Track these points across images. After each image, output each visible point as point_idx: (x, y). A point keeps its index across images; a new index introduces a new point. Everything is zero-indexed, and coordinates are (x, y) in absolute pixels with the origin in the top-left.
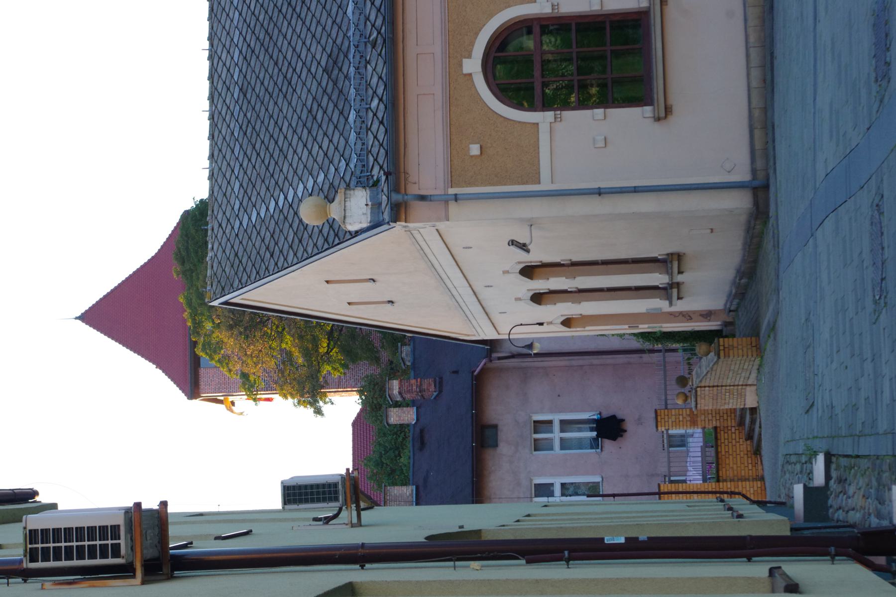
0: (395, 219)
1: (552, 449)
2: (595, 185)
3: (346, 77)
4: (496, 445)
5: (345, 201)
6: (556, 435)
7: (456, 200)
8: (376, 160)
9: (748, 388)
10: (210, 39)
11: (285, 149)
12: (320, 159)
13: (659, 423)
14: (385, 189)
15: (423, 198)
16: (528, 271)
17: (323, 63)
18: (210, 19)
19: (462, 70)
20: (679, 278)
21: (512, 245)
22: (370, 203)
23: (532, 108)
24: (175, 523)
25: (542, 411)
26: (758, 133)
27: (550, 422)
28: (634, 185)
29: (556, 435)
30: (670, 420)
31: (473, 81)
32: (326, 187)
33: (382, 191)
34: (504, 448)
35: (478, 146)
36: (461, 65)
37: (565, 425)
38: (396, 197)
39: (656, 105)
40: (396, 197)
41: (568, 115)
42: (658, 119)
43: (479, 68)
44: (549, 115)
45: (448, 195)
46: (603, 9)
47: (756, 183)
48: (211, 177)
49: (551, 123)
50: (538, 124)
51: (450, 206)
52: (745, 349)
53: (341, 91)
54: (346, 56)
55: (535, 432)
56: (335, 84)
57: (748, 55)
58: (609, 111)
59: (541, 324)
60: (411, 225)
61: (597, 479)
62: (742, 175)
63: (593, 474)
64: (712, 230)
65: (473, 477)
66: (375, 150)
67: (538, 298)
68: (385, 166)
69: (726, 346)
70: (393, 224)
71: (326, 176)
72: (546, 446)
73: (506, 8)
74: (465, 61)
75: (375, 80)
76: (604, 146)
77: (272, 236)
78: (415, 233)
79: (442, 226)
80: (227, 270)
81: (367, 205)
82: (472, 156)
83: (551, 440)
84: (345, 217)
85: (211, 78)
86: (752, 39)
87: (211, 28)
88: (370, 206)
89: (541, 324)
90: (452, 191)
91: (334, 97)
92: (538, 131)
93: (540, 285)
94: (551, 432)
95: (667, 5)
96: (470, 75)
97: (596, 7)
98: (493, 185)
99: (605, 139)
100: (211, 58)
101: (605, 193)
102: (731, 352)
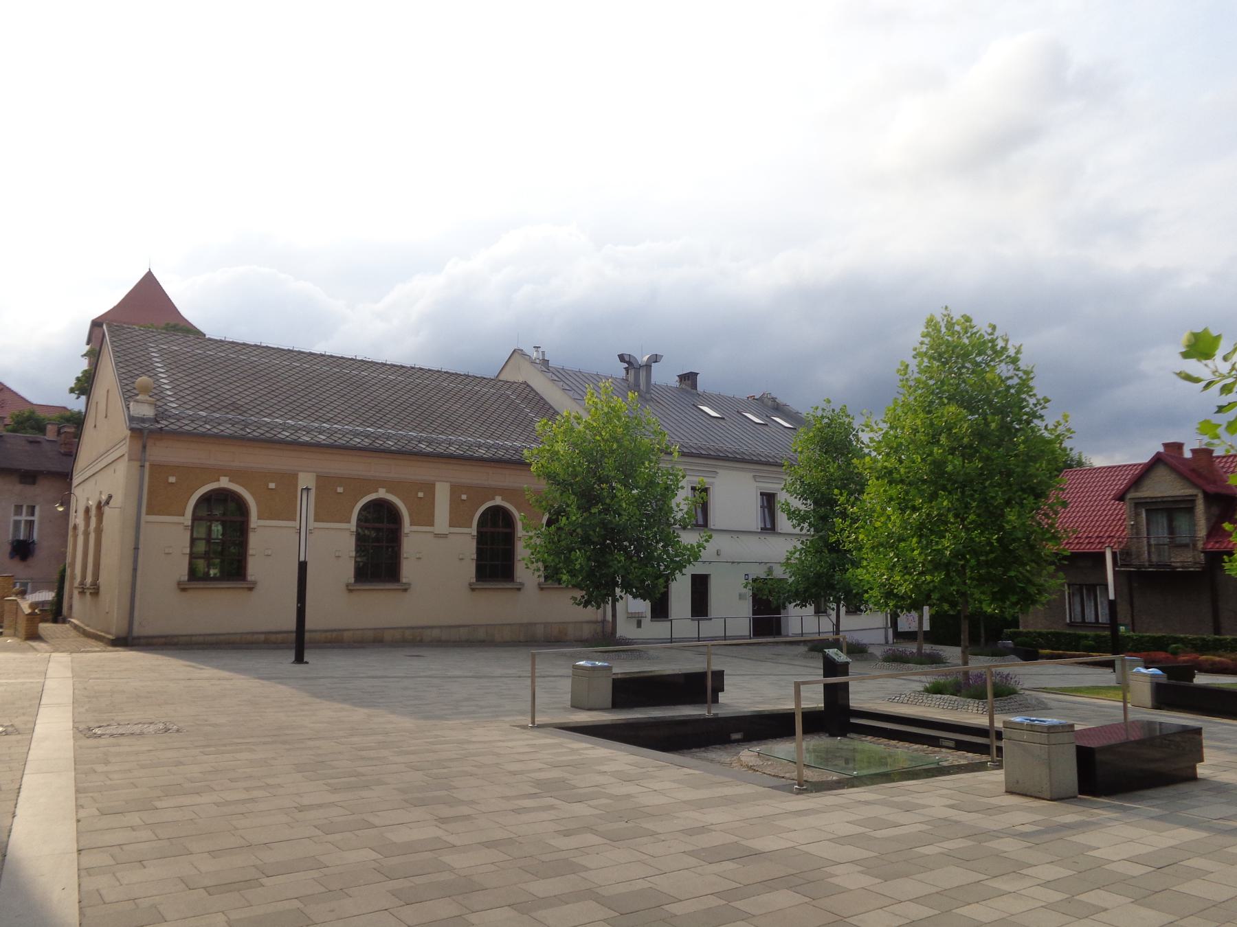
0: (132, 429)
3: (227, 413)
4: (21, 482)
7: (141, 466)
8: (172, 423)
10: (267, 347)
11: (192, 376)
12: (181, 394)
15: (144, 447)
16: (99, 507)
17: (238, 402)
18: (278, 348)
20: (88, 594)
23: (359, 520)
26: (163, 640)
27: (33, 514)
29: (24, 517)
32: (162, 395)
34: (18, 487)
35: (342, 491)
37: (30, 524)
40: (146, 432)
41: (475, 542)
42: (347, 586)
44: (475, 533)
53: (219, 409)
54: (240, 414)
56: (224, 407)
57: (186, 636)
58: (475, 561)
59: (76, 512)
60: (128, 440)
62: (137, 631)
64: (107, 613)
66: (179, 424)
67: (87, 510)
68: (167, 428)
71: (169, 395)
72: (18, 509)
74: (384, 490)
75: (222, 428)
77: (140, 362)
78: (124, 442)
79: (126, 457)
80: (124, 336)
83: (21, 514)
85: (244, 344)
87: (273, 349)
89: (76, 512)
90: (147, 465)
91: (217, 406)
93: (93, 512)
96: (219, 481)
97: (251, 552)
99: (170, 554)
100: (256, 346)
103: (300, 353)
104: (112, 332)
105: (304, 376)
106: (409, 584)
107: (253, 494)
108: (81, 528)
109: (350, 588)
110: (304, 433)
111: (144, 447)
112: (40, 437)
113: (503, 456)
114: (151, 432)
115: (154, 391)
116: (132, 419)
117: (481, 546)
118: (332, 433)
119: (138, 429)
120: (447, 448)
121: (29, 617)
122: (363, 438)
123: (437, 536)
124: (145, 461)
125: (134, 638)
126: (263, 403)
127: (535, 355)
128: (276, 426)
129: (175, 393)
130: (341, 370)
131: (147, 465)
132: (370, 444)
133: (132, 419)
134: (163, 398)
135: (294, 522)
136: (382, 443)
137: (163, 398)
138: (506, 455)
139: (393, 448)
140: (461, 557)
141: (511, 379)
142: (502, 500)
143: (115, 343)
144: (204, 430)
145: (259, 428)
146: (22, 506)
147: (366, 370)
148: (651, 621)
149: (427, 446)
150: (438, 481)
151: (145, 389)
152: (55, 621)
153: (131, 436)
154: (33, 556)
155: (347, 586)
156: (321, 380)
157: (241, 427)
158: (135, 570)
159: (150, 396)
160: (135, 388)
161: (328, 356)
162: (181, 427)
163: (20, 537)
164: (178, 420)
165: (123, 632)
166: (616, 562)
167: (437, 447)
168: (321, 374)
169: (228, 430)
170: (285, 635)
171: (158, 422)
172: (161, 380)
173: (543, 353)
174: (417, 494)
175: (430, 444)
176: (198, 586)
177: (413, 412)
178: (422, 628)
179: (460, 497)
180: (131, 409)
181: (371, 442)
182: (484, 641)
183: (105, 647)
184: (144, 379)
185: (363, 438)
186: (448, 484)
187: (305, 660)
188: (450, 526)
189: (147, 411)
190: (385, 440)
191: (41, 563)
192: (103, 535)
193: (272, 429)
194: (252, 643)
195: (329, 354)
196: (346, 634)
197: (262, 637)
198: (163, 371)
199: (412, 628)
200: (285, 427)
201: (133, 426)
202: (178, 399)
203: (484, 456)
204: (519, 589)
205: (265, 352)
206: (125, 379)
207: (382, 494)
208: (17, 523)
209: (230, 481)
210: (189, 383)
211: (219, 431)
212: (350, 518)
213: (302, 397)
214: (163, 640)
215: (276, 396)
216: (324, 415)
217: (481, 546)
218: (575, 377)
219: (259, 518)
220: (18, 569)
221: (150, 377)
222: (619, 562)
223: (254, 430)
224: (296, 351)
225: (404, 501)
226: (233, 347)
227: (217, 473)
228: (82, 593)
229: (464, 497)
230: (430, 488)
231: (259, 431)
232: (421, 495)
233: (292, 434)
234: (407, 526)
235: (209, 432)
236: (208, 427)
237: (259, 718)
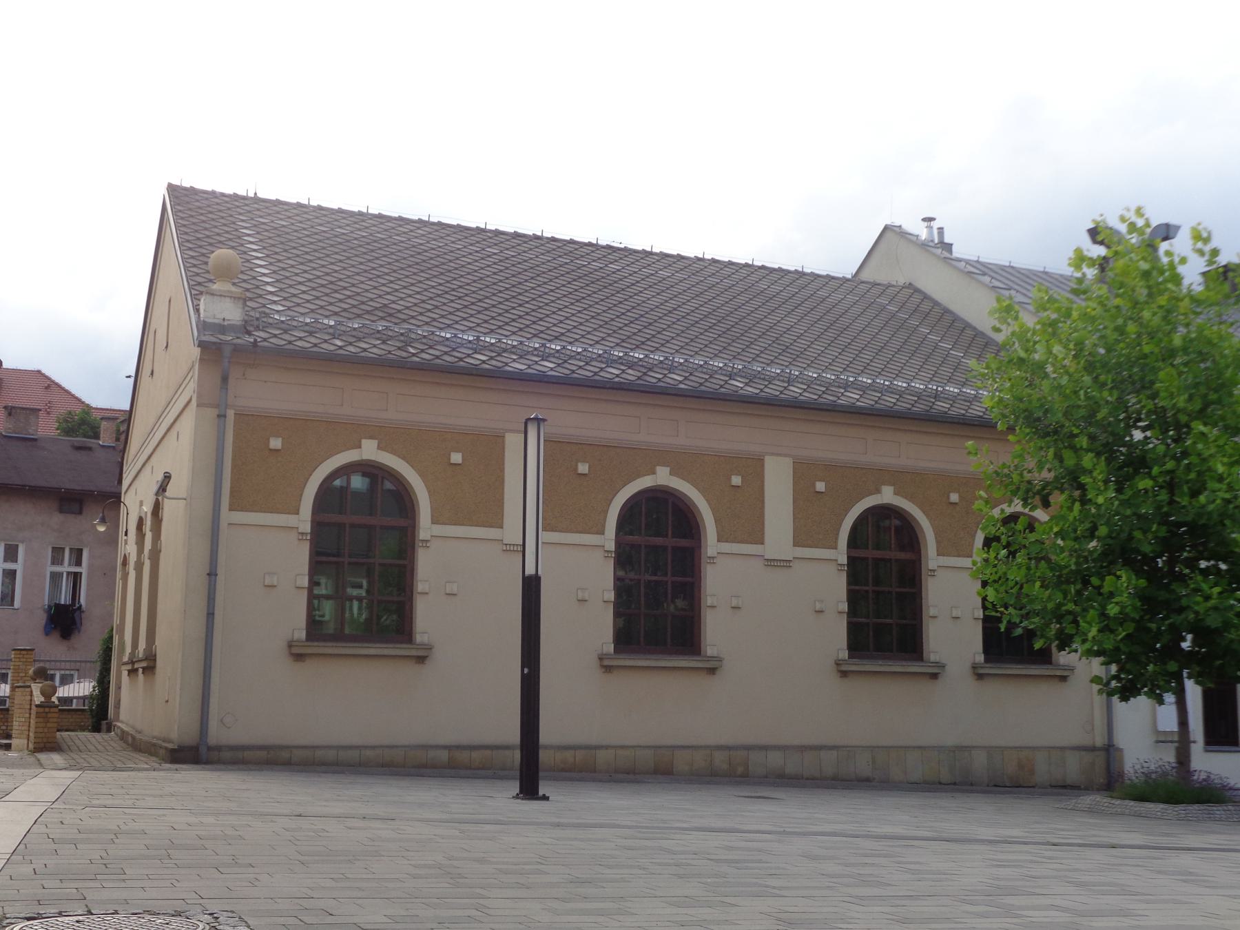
0: (202, 345)
1: (53, 563)
2: (221, 571)
4: (61, 511)
5: (231, 297)
6: (66, 568)
7: (219, 416)
9: (26, 742)
10: (440, 224)
13: (19, 652)
14: (239, 341)
15: (225, 379)
18: (459, 226)
19: (365, 438)
21: (165, 477)
22: (226, 323)
24: (546, 747)
25: (91, 557)
27: (79, 563)
28: (216, 612)
30: (20, 663)
31: (353, 448)
33: (238, 338)
34: (57, 519)
35: (823, 490)
36: (371, 438)
37: (76, 577)
38: (227, 351)
39: (309, 644)
40: (227, 351)
42: (290, 645)
43: (365, 457)
44: (307, 528)
45: (226, 408)
46: (418, 595)
47: (203, 750)
48: (299, 205)
49: (297, 528)
50: (298, 514)
51: (210, 409)
52: (43, 735)
55: (71, 549)
56: (368, 312)
61: (17, 604)
62: (217, 734)
63: (22, 601)
65: (29, 486)
66: (287, 337)
69: (49, 715)
70: (196, 342)
73: (429, 492)
76: (266, 584)
81: (224, 319)
82: (268, 439)
83: (62, 563)
84: (213, 294)
85: (401, 219)
86: (368, 753)
88: (222, 322)
89: (126, 535)
90: (231, 414)
92: (289, 513)
94: (70, 565)
95: (416, 663)
96: (360, 447)
97: (420, 587)
98: (233, 460)
101: (210, 581)
102: (41, 720)
103: (498, 233)
104: (177, 197)
105: (507, 268)
106: (719, 659)
107: (422, 475)
108: (133, 559)
109: (606, 663)
110: (515, 357)
111: (225, 379)
112: (91, 442)
113: (895, 404)
114: (237, 349)
115: (241, 276)
116: (204, 326)
117: (853, 587)
118: (563, 358)
119: (214, 343)
120: (785, 388)
121: (41, 710)
122: (623, 368)
123: (771, 563)
124: (227, 406)
125: (210, 748)
126: (437, 307)
127: (924, 234)
128: (462, 345)
129: (281, 290)
130: (572, 261)
131: (231, 414)
132: (639, 378)
133: (204, 326)
134: (261, 296)
135: (499, 530)
136: (660, 376)
137: (261, 296)
138: (899, 403)
139: (682, 386)
140: (818, 607)
141: (882, 278)
142: (895, 494)
143: (180, 214)
144: (332, 348)
145: (431, 347)
146: (63, 549)
147: (616, 261)
148: (1207, 751)
149: (747, 384)
150: (773, 454)
151: (225, 272)
152: (96, 729)
153: (201, 359)
154: (79, 632)
155: (601, 659)
156: (538, 275)
157: (399, 344)
158: (210, 615)
159: (234, 284)
160: (208, 272)
161: (547, 238)
162: (290, 342)
163: (60, 599)
164: (286, 331)
165: (190, 738)
166: (1199, 599)
167: (766, 386)
168: (538, 266)
169: (375, 349)
170: (488, 752)
171: (249, 333)
172: (258, 270)
173: (941, 230)
174: (730, 479)
175: (751, 379)
176: (321, 651)
177: (710, 327)
178: (748, 748)
179: (814, 486)
180: (202, 308)
181: (639, 374)
182: (868, 780)
183: (160, 764)
184: (222, 254)
185: (623, 368)
186: (788, 462)
187: (541, 793)
188: (795, 545)
189: (228, 312)
190: (666, 372)
191: (88, 643)
192: (43, 372)
193: (454, 350)
194: (425, 766)
195: (549, 236)
196: (602, 756)
197: (444, 756)
198: (260, 255)
199: (729, 748)
200: (478, 347)
201: (204, 338)
202: (285, 299)
203: (858, 403)
204: (934, 676)
205: (437, 231)
206: (195, 266)
207: (663, 477)
208: (56, 577)
209: (379, 448)
210: (306, 275)
211: (359, 350)
212: (604, 526)
213: (507, 300)
214: (263, 754)
215: (460, 298)
216: (548, 328)
217: (853, 587)
218: (1004, 274)
219: (435, 521)
220: (53, 650)
221: (233, 248)
222: (1207, 598)
223: (423, 351)
224: (490, 231)
225: (703, 492)
226: (382, 223)
227: (355, 431)
228: (132, 672)
229: (820, 486)
230: (754, 468)
231: (431, 351)
232: (736, 480)
233: (492, 358)
234: (711, 543)
235: (341, 352)
236: (339, 343)
237: (474, 913)
